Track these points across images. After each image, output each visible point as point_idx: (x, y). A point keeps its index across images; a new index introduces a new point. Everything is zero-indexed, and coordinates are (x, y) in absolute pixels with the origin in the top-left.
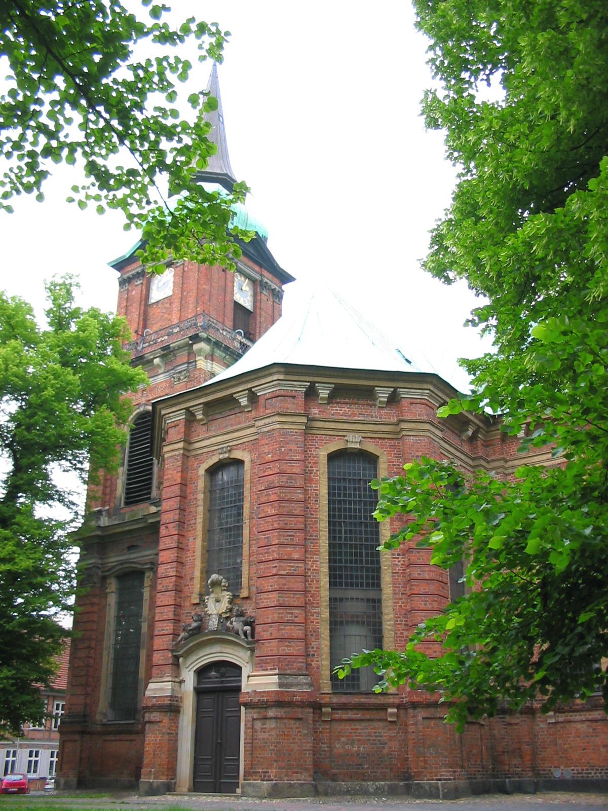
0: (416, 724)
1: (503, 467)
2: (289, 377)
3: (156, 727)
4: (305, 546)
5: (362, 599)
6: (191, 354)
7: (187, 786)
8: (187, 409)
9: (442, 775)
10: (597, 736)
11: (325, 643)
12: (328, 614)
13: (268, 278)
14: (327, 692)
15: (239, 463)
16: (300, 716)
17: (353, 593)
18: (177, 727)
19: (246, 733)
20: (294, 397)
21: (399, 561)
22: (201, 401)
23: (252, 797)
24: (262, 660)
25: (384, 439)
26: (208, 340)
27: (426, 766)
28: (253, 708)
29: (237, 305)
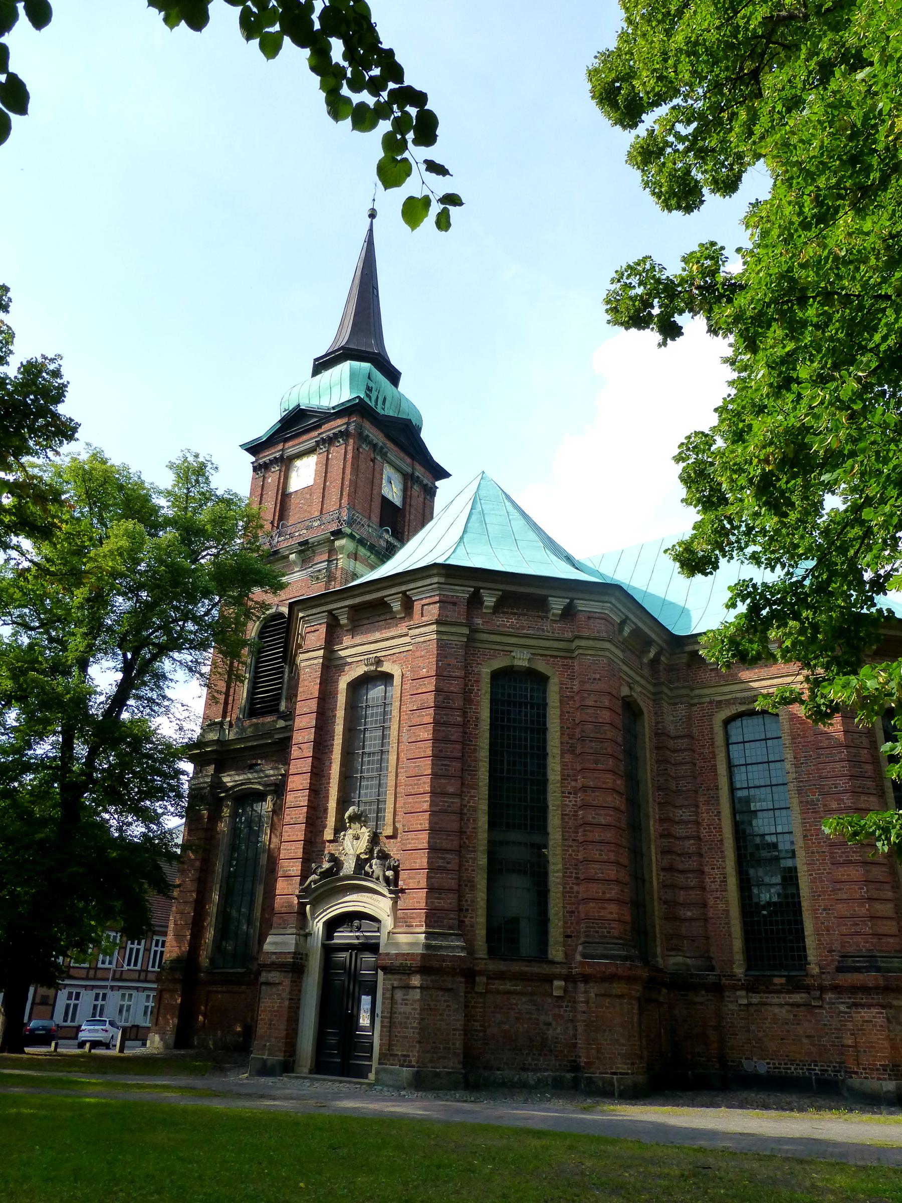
0: (587, 1002)
1: (688, 696)
2: (450, 581)
3: (274, 990)
4: (462, 778)
5: (526, 844)
6: (332, 551)
7: (309, 1066)
8: (330, 612)
9: (617, 1068)
10: (798, 1024)
11: (481, 896)
12: (485, 861)
13: (420, 471)
14: (481, 956)
15: (387, 678)
16: (450, 986)
17: (514, 836)
18: (300, 991)
19: (383, 1003)
20: (455, 604)
21: (570, 801)
22: (347, 603)
23: (389, 1086)
24: (406, 914)
25: (556, 657)
26: (351, 536)
27: (600, 1055)
28: (393, 974)
29: (385, 501)
